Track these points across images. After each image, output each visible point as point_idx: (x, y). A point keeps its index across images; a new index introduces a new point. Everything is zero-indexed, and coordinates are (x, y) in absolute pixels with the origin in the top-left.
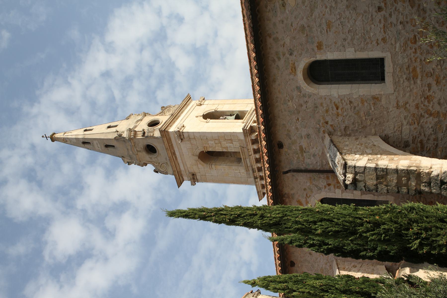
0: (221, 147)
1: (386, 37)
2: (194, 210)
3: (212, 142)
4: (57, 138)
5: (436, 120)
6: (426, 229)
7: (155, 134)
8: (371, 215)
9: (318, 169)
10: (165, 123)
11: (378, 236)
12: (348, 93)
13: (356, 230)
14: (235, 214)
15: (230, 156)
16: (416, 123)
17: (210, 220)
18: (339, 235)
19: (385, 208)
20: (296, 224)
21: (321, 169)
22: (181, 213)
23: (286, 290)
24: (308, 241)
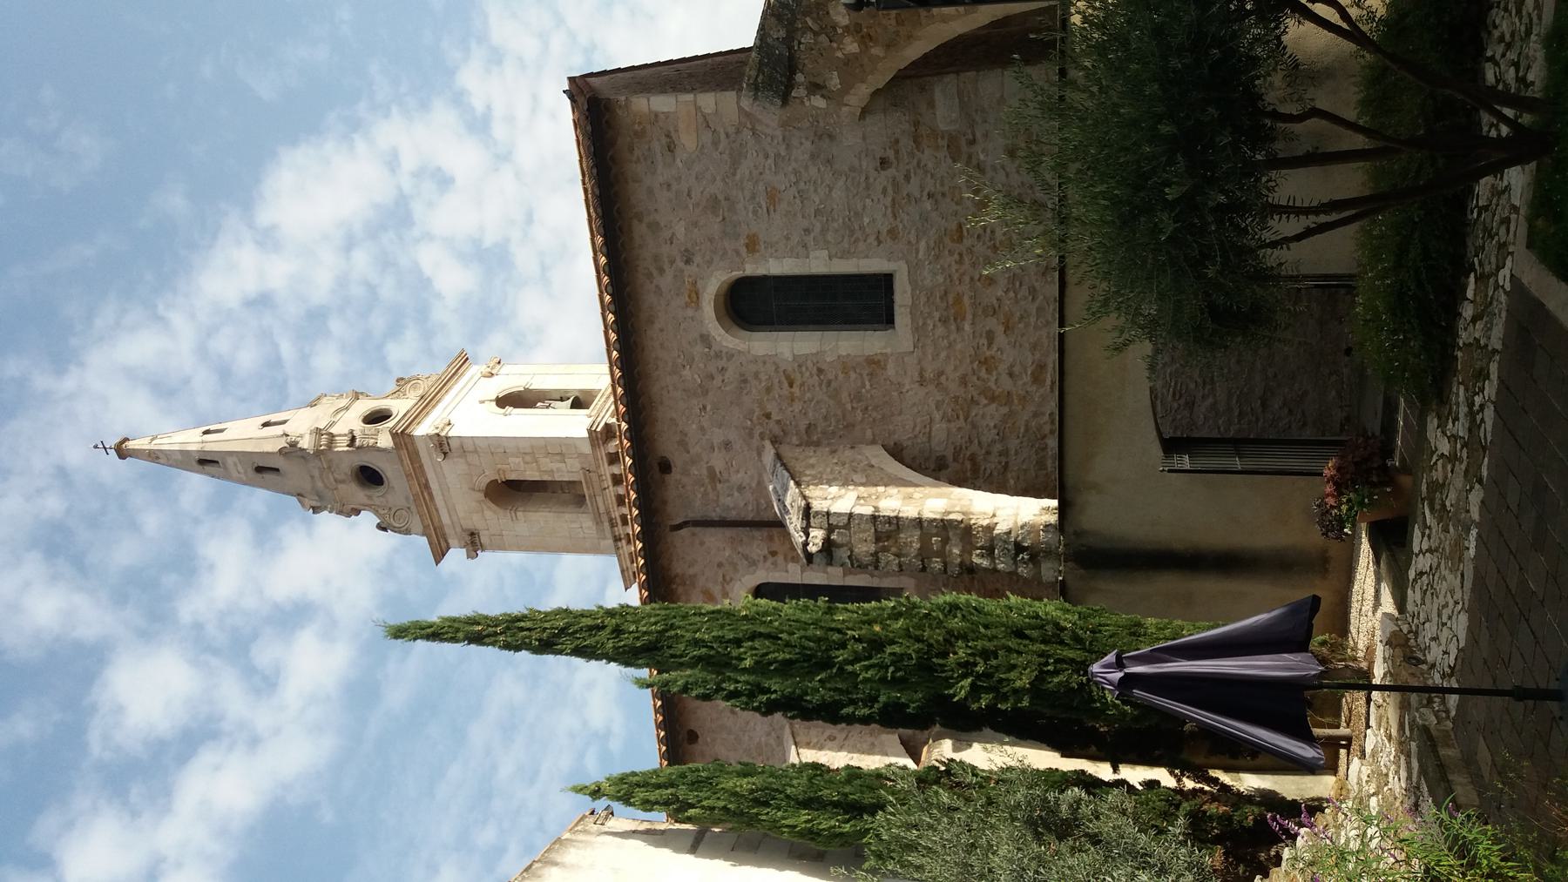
0: (539, 470)
1: (897, 226)
2: (454, 620)
3: (517, 460)
4: (133, 449)
5: (1005, 410)
6: (986, 655)
7: (379, 442)
8: (864, 622)
9: (750, 519)
10: (405, 415)
11: (879, 671)
12: (814, 351)
13: (830, 658)
14: (554, 628)
15: (560, 492)
16: (961, 417)
17: (493, 644)
18: (794, 671)
19: (894, 607)
20: (696, 647)
21: (756, 519)
22: (424, 629)
23: (671, 804)
24: (724, 685)
